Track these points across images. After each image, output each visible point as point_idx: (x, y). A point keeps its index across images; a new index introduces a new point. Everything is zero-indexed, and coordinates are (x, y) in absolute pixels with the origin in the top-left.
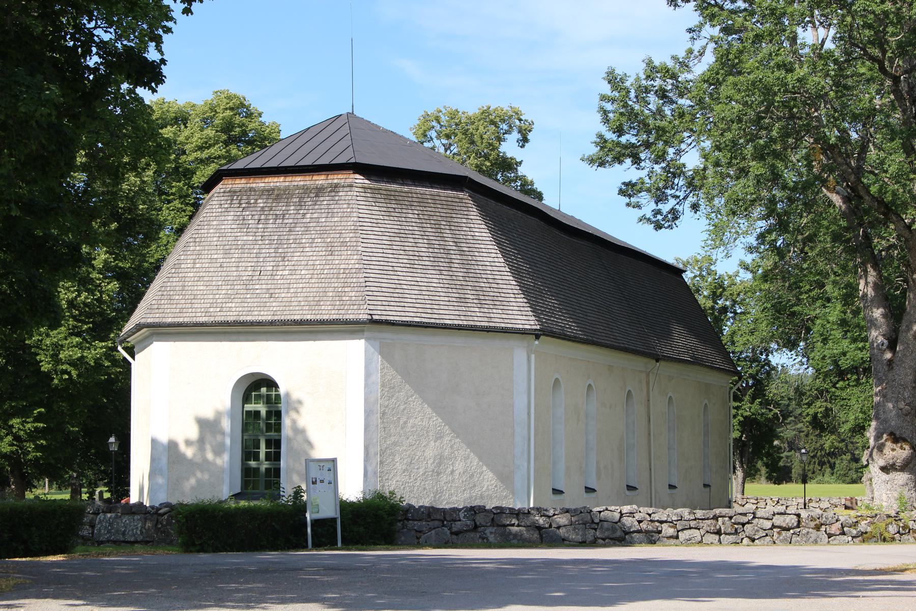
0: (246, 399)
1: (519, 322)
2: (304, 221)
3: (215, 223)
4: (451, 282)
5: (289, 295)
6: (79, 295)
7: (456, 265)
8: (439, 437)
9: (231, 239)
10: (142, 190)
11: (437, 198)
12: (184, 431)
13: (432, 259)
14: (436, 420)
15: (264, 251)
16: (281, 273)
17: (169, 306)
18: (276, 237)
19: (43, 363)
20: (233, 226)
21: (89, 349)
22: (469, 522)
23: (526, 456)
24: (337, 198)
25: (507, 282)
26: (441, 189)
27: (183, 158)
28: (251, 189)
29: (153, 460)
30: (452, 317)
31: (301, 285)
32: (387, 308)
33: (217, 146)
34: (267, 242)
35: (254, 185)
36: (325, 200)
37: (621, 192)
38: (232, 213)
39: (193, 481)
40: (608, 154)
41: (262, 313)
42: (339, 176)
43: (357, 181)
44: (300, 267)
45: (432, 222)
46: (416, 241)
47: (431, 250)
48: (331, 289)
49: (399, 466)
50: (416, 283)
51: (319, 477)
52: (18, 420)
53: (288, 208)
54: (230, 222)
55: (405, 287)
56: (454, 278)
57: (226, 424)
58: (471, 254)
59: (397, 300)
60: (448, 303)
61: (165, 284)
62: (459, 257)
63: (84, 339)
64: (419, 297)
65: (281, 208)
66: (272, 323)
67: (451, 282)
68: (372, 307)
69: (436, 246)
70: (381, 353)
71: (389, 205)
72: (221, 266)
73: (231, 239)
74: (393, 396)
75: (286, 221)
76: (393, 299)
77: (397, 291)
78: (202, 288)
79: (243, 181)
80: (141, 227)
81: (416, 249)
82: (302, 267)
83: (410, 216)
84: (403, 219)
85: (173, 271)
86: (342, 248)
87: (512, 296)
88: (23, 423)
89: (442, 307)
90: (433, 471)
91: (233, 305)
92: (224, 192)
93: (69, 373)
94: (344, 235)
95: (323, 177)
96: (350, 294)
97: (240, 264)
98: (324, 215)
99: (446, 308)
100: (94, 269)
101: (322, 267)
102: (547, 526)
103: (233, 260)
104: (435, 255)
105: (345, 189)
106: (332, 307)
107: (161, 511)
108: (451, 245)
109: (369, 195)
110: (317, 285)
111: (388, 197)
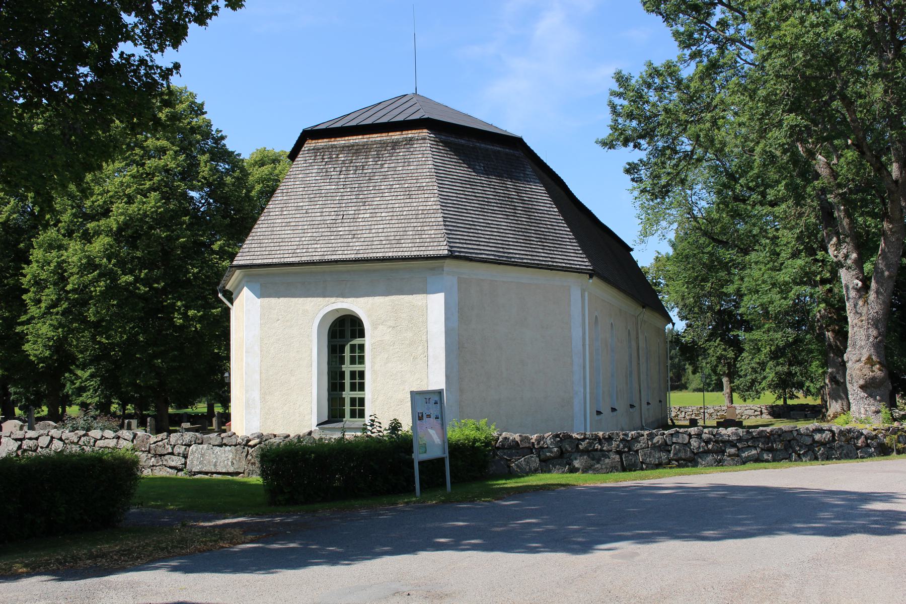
5: (371, 235)
16: (362, 216)
28: (333, 147)
31: (382, 226)
36: (401, 152)
37: (628, 171)
48: (410, 229)
51: (426, 412)
96: (430, 232)
107: (251, 443)
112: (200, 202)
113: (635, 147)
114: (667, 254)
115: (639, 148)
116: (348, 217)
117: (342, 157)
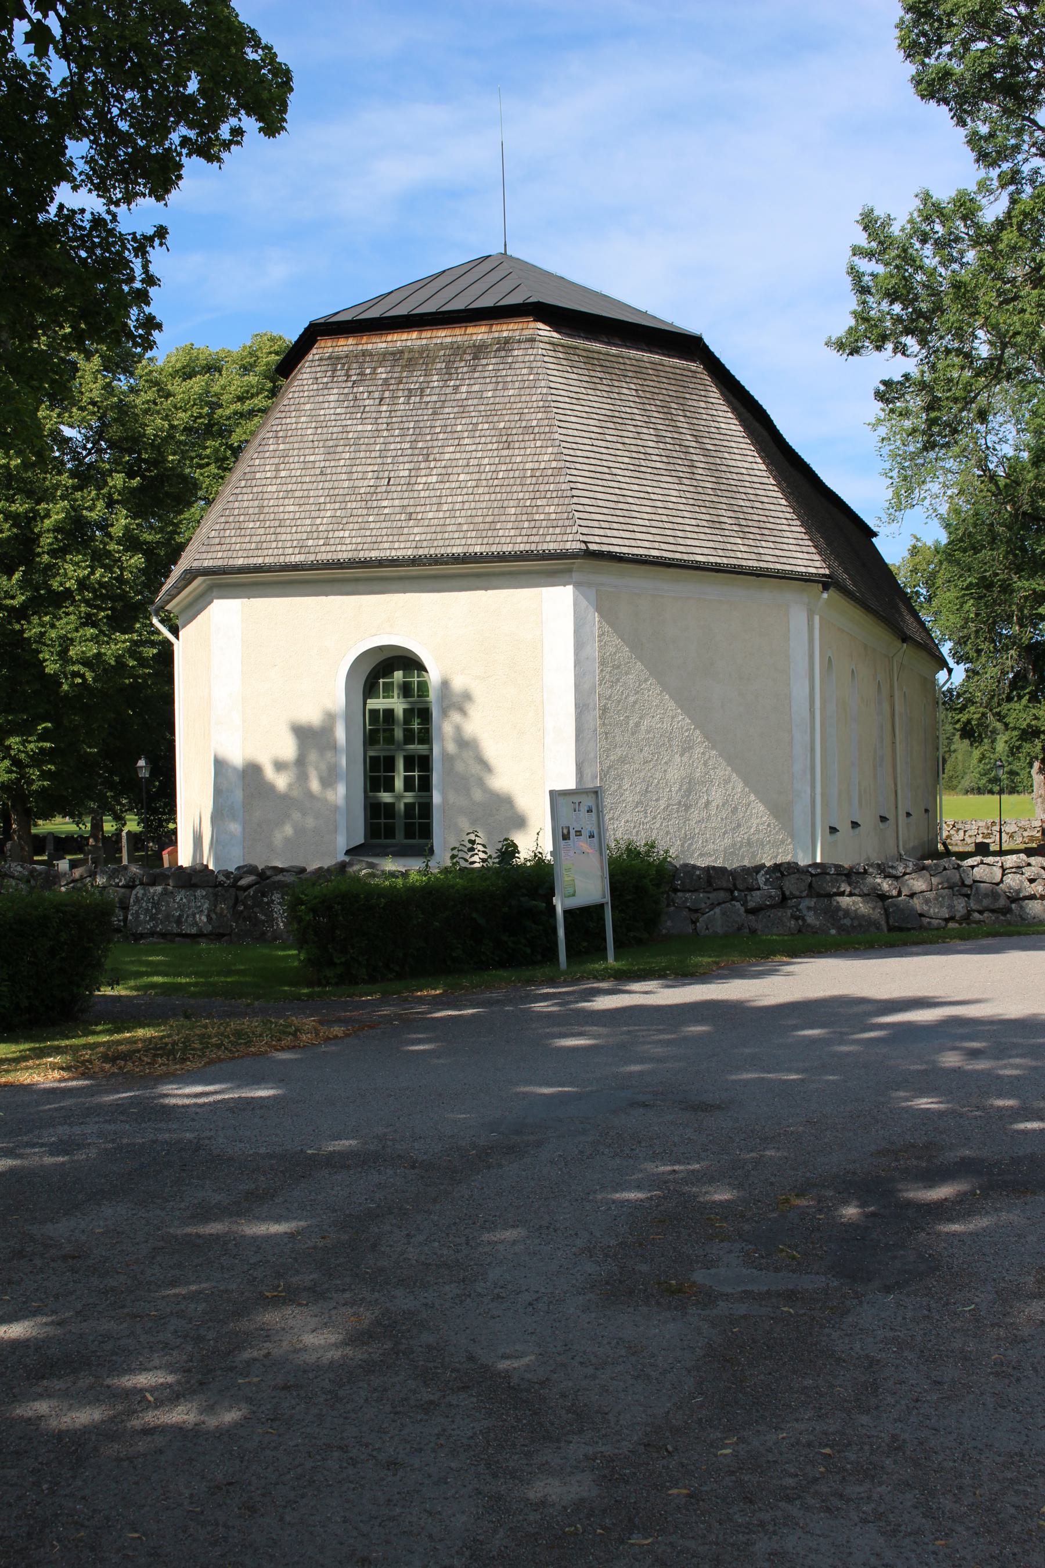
0: (370, 689)
1: (800, 562)
2: (458, 396)
3: (308, 407)
4: (696, 496)
5: (441, 514)
6: (92, 573)
7: (700, 471)
8: (687, 748)
9: (335, 430)
10: (171, 437)
11: (660, 368)
12: (271, 747)
13: (665, 459)
14: (683, 721)
15: (392, 447)
17: (239, 540)
18: (412, 425)
19: (48, 663)
20: (338, 411)
21: (108, 643)
22: (773, 892)
23: (809, 776)
24: (510, 360)
25: (775, 501)
26: (664, 355)
27: (219, 411)
28: (364, 353)
29: (218, 792)
30: (706, 551)
31: (460, 499)
32: (609, 533)
33: (260, 396)
34: (397, 432)
35: (370, 347)
36: (490, 364)
37: (880, 396)
38: (335, 391)
39: (288, 830)
40: (864, 336)
41: (396, 545)
42: (511, 327)
43: (541, 333)
44: (455, 470)
45: (658, 403)
46: (639, 430)
47: (661, 446)
48: (512, 503)
49: (630, 797)
50: (646, 496)
52: (18, 739)
53: (428, 379)
54: (332, 405)
55: (630, 500)
56: (700, 490)
57: (340, 734)
58: (720, 455)
59: (621, 520)
60: (696, 529)
61: (230, 505)
62: (702, 459)
63: (101, 631)
64: (654, 517)
65: (417, 378)
66: (414, 561)
67: (696, 496)
68: (585, 530)
69: (668, 440)
70: (599, 609)
71: (592, 373)
72: (322, 474)
73: (335, 430)
74: (618, 680)
75: (426, 399)
76: (615, 519)
77: (620, 506)
78: (292, 508)
79: (351, 341)
80: (171, 485)
81: (639, 442)
82: (459, 470)
83: (625, 391)
84: (616, 396)
85: (243, 483)
86: (526, 437)
87: (784, 521)
88: (24, 743)
89: (689, 535)
90: (679, 803)
91: (347, 533)
92: (321, 359)
93: (82, 676)
94: (528, 417)
95: (483, 329)
97: (354, 469)
98: (490, 387)
99: (695, 536)
100: (111, 540)
101: (493, 468)
102: (894, 893)
103: (342, 463)
104: (668, 453)
105: (523, 346)
106: (517, 532)
107: (243, 882)
108: (689, 440)
109: (561, 355)
110: (487, 497)
111: (590, 360)
112: (85, 448)
113: (895, 351)
114: (937, 542)
115: (904, 354)
116: (397, 481)
117: (382, 373)
